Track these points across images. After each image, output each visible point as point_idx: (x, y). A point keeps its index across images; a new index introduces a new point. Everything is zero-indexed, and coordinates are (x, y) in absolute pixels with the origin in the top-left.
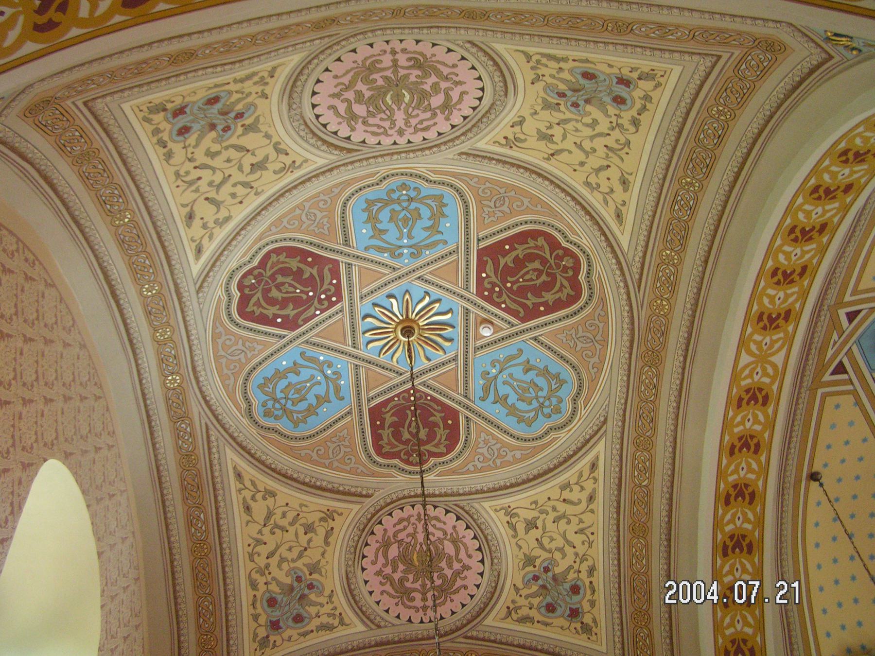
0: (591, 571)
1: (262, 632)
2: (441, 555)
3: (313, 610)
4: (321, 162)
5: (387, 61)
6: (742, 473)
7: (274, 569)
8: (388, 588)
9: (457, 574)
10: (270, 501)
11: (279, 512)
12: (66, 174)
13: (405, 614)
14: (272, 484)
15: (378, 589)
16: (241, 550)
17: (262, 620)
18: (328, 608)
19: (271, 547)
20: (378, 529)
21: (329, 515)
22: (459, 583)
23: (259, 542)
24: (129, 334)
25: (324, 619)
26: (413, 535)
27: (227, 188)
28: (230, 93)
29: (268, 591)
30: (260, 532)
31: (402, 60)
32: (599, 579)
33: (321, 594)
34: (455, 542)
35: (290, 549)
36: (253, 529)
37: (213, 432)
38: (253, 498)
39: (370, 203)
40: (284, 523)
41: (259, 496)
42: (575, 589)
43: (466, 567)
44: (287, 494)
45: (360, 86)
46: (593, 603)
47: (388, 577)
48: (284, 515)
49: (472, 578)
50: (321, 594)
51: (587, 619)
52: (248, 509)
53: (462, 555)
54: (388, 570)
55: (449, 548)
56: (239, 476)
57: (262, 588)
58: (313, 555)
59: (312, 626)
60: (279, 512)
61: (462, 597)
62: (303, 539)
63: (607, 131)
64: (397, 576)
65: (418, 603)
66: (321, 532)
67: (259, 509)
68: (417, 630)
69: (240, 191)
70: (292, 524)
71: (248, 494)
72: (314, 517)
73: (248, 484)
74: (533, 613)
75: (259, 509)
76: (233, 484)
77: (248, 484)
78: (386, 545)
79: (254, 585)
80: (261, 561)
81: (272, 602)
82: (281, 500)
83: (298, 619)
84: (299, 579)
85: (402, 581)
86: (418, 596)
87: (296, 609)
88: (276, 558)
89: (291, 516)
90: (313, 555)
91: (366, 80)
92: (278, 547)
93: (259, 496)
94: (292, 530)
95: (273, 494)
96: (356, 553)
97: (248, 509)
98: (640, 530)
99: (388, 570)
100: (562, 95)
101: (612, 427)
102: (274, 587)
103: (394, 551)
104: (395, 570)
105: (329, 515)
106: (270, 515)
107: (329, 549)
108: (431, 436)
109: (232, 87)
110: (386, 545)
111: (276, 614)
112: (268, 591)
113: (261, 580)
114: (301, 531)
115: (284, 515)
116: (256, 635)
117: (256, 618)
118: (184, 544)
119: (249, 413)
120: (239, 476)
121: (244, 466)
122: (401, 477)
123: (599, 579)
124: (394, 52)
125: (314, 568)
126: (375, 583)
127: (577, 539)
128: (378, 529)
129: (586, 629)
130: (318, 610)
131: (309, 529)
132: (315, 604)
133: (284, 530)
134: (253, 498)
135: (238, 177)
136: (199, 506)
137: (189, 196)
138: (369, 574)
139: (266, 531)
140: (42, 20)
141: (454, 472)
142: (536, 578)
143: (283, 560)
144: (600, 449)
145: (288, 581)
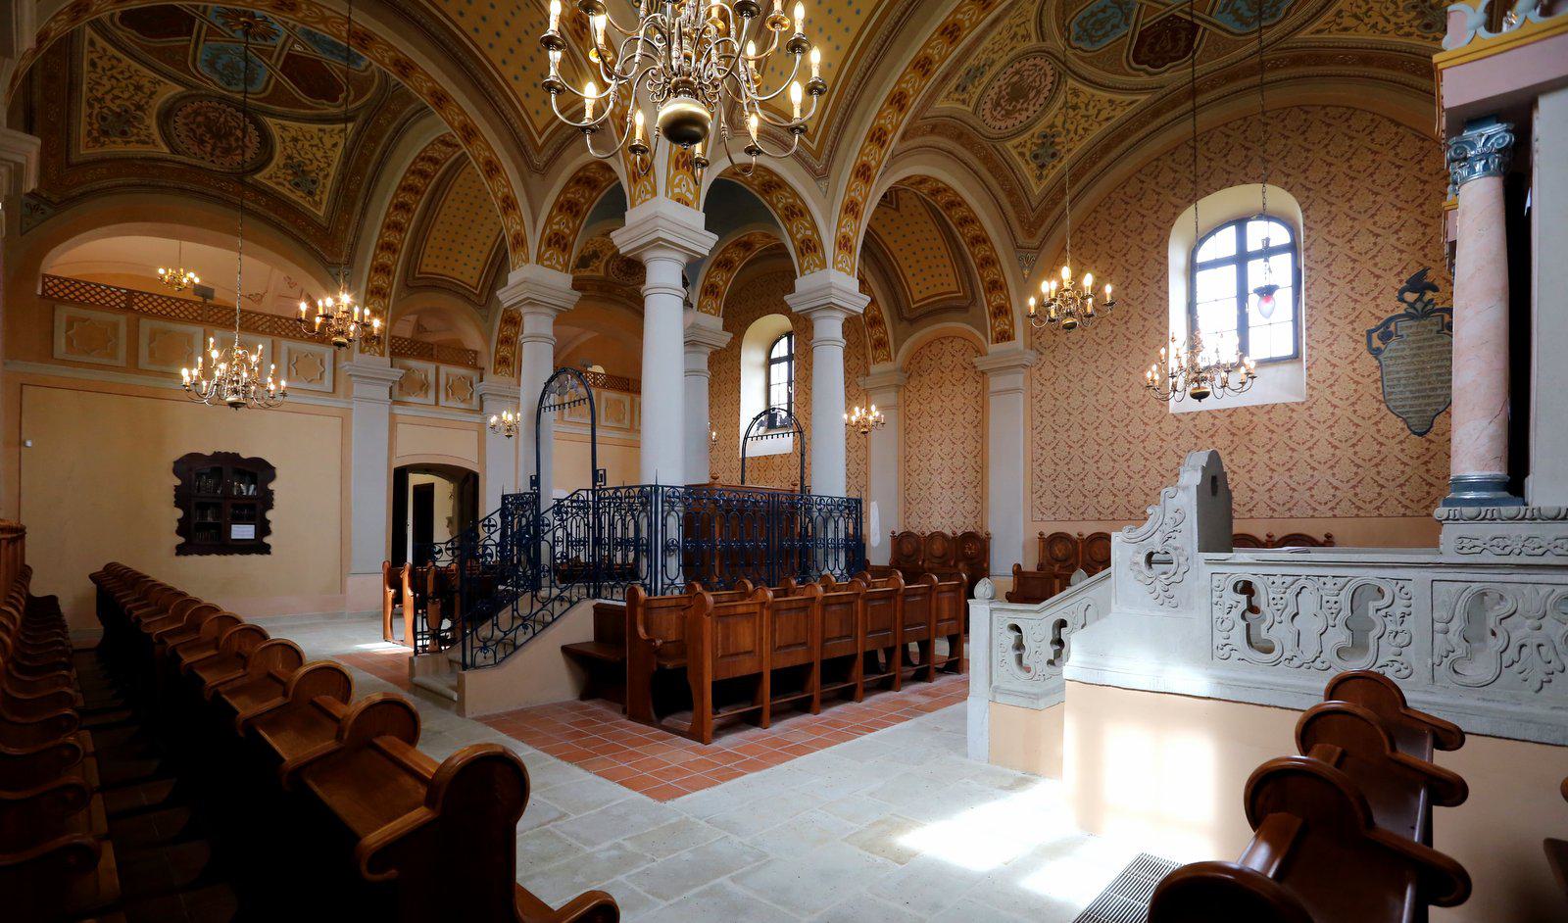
4: (1301, 36)
5: (217, 152)
7: (1399, 21)
11: (1355, 10)
16: (1377, 37)
23: (1375, 26)
24: (991, 673)
27: (313, 142)
28: (289, 182)
29: (1417, 27)
30: (1366, 25)
31: (208, 148)
35: (1387, 9)
38: (1339, 25)
41: (1338, 20)
43: (1027, 110)
45: (234, 145)
46: (1054, 167)
48: (1358, 7)
51: (1044, 173)
52: (1346, 29)
56: (1319, 32)
57: (1413, 29)
60: (1355, 10)
61: (1010, 122)
67: (1347, 21)
69: (308, 136)
71: (1335, 27)
73: (1327, 26)
77: (1327, 26)
79: (1409, 35)
80: (1390, 27)
85: (1003, 97)
91: (231, 145)
92: (1383, 16)
93: (1338, 20)
95: (1341, 11)
97: (1346, 29)
100: (1053, 136)
102: (1416, 23)
106: (1355, 16)
109: (287, 184)
112: (1417, 27)
113: (1407, 29)
115: (1358, 7)
120: (1319, 32)
121: (1317, 25)
124: (212, 155)
129: (1040, 177)
132: (1059, 144)
134: (1339, 25)
135: (307, 144)
137: (330, 153)
139: (1366, 20)
143: (1394, 14)
145: (1413, 14)
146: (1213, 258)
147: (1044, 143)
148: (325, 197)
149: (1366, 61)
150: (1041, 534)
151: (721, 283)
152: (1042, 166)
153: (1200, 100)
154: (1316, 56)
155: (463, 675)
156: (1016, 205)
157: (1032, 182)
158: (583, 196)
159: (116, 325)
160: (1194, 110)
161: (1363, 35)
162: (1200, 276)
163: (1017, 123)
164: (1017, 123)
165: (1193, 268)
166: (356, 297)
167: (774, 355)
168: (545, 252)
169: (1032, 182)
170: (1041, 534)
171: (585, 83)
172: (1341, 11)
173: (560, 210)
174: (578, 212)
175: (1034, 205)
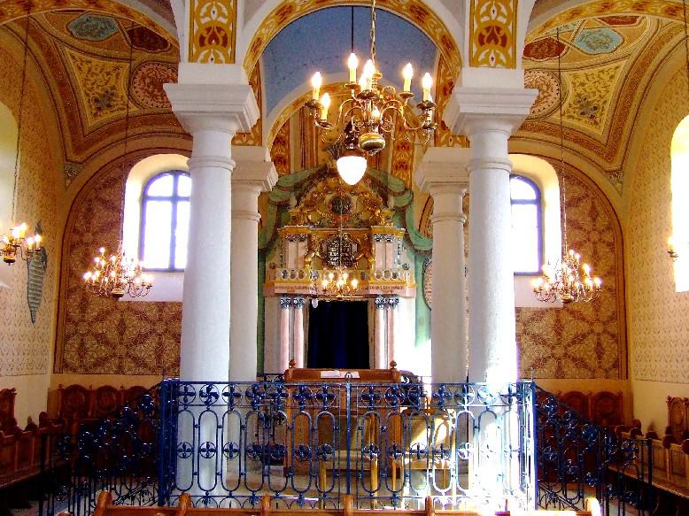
0: (605, 102)
1: (94, 112)
6: (493, 16)
12: (651, 68)
16: (80, 83)
32: (607, 107)
33: (118, 97)
40: (98, 72)
41: (84, 63)
42: (595, 108)
44: (95, 61)
51: (598, 120)
52: (80, 68)
56: (73, 57)
58: (112, 83)
63: (630, 13)
64: (150, 90)
67: (85, 68)
70: (100, 72)
74: (575, 115)
75: (85, 68)
76: (71, 61)
78: (143, 78)
79: (88, 95)
83: (109, 106)
90: (112, 83)
96: (130, 84)
97: (80, 68)
98: (634, 85)
101: (632, 59)
102: (96, 95)
104: (149, 87)
107: (119, 81)
111: (99, 105)
113: (91, 93)
116: (91, 113)
117: (90, 106)
120: (73, 57)
121: (77, 55)
123: (607, 107)
125: (113, 88)
126: (141, 92)
127: (602, 90)
130: (118, 103)
131: (108, 74)
133: (97, 75)
136: (58, 70)
140: (500, 42)
142: (579, 102)
144: (623, 63)
146: (537, 230)
148: (605, 117)
151: (502, 20)
152: (99, 109)
157: (89, 116)
162: (149, 204)
164: (150, 103)
165: (144, 198)
166: (584, 254)
170: (60, 386)
171: (316, 71)
172: (90, 62)
173: (481, 42)
175: (86, 133)
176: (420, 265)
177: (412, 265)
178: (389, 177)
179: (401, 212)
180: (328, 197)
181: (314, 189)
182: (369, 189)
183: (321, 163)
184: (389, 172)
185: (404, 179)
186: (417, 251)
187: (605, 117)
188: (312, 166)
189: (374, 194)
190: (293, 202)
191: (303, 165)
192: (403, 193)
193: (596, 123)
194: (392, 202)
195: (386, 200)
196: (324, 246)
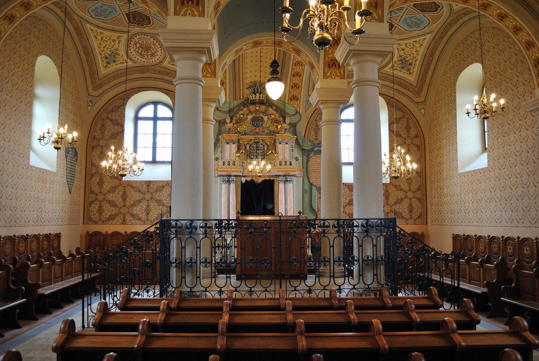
1: (105, 65)
2: (151, 47)
3: (118, 59)
4: (88, 25)
8: (137, 54)
9: (155, 52)
10: (102, 35)
11: (105, 37)
13: (143, 60)
14: (102, 31)
15: (135, 54)
17: (105, 62)
18: (122, 59)
19: (104, 45)
20: (133, 40)
21: (119, 37)
22: (156, 54)
23: (100, 45)
25: (121, 61)
26: (143, 42)
33: (119, 55)
34: (154, 45)
36: (98, 42)
37: (82, 21)
39: (105, 17)
42: (410, 64)
44: (106, 33)
47: (137, 51)
49: (159, 53)
50: (119, 55)
51: (411, 71)
52: (96, 37)
53: (156, 48)
54: (137, 50)
55: (153, 46)
56: (92, 30)
59: (118, 63)
60: (105, 37)
61: (157, 57)
62: (113, 43)
64: (140, 51)
65: (146, 58)
66: (117, 41)
67: (99, 37)
68: (146, 64)
71: (95, 34)
72: (114, 38)
75: (99, 37)
76: (91, 32)
79: (101, 54)
80: (102, 49)
81: (106, 58)
82: (104, 34)
83: (114, 61)
84: (113, 52)
86: (146, 56)
87: (113, 59)
88: (106, 48)
89: (108, 38)
90: (116, 47)
94: (109, 41)
95: (102, 33)
97: (96, 37)
99: (137, 50)
102: (106, 54)
103: (138, 45)
105: (119, 37)
108: (144, 21)
110: (136, 44)
111: (108, 60)
113: (103, 53)
114: (112, 41)
118: (80, 47)
119: (91, 16)
120: (92, 30)
121: (92, 27)
122: (137, 28)
125: (117, 50)
126: (134, 53)
128: (133, 40)
130: (119, 59)
131: (114, 41)
138: (132, 50)
141: (151, 29)
143: (108, 48)
147: (111, 55)
148: (415, 70)
149: (85, 47)
150: (88, 232)
153: (129, 77)
154: (81, 33)
155: (349, 5)
156: (92, 75)
158: (298, 80)
159: (466, 268)
160: (126, 80)
161: (95, 43)
163: (135, 56)
164: (140, 59)
167: (141, 114)
168: (328, 72)
169: (102, 68)
170: (88, 232)
174: (297, 99)
176: (305, 158)
177: (300, 158)
178: (287, 105)
179: (293, 126)
180: (250, 117)
181: (241, 112)
182: (275, 112)
183: (245, 96)
184: (287, 102)
185: (296, 106)
186: (303, 149)
187: (416, 70)
188: (243, 97)
189: (277, 115)
190: (228, 120)
191: (235, 99)
192: (295, 115)
193: (410, 73)
194: (288, 121)
195: (284, 118)
196: (248, 147)
